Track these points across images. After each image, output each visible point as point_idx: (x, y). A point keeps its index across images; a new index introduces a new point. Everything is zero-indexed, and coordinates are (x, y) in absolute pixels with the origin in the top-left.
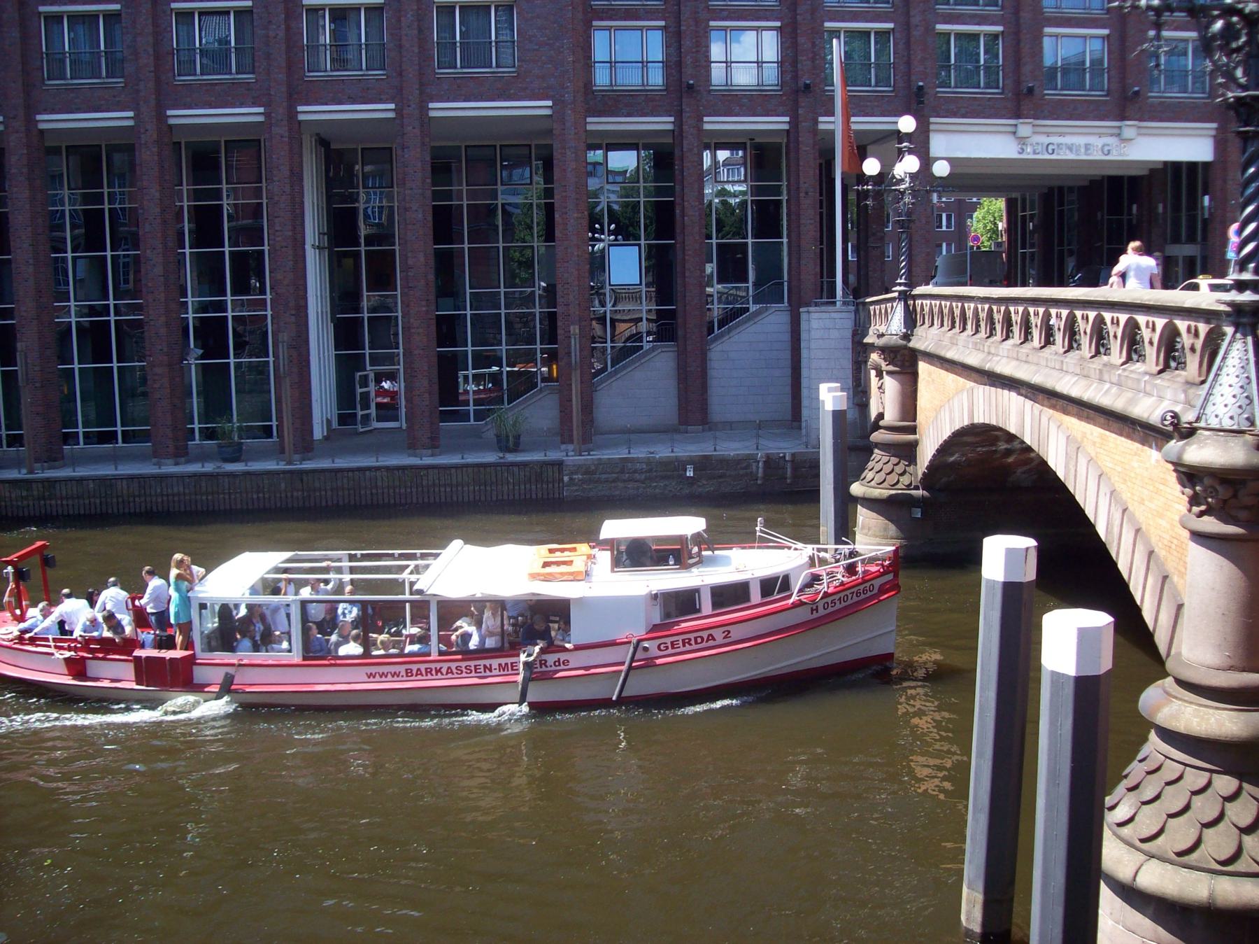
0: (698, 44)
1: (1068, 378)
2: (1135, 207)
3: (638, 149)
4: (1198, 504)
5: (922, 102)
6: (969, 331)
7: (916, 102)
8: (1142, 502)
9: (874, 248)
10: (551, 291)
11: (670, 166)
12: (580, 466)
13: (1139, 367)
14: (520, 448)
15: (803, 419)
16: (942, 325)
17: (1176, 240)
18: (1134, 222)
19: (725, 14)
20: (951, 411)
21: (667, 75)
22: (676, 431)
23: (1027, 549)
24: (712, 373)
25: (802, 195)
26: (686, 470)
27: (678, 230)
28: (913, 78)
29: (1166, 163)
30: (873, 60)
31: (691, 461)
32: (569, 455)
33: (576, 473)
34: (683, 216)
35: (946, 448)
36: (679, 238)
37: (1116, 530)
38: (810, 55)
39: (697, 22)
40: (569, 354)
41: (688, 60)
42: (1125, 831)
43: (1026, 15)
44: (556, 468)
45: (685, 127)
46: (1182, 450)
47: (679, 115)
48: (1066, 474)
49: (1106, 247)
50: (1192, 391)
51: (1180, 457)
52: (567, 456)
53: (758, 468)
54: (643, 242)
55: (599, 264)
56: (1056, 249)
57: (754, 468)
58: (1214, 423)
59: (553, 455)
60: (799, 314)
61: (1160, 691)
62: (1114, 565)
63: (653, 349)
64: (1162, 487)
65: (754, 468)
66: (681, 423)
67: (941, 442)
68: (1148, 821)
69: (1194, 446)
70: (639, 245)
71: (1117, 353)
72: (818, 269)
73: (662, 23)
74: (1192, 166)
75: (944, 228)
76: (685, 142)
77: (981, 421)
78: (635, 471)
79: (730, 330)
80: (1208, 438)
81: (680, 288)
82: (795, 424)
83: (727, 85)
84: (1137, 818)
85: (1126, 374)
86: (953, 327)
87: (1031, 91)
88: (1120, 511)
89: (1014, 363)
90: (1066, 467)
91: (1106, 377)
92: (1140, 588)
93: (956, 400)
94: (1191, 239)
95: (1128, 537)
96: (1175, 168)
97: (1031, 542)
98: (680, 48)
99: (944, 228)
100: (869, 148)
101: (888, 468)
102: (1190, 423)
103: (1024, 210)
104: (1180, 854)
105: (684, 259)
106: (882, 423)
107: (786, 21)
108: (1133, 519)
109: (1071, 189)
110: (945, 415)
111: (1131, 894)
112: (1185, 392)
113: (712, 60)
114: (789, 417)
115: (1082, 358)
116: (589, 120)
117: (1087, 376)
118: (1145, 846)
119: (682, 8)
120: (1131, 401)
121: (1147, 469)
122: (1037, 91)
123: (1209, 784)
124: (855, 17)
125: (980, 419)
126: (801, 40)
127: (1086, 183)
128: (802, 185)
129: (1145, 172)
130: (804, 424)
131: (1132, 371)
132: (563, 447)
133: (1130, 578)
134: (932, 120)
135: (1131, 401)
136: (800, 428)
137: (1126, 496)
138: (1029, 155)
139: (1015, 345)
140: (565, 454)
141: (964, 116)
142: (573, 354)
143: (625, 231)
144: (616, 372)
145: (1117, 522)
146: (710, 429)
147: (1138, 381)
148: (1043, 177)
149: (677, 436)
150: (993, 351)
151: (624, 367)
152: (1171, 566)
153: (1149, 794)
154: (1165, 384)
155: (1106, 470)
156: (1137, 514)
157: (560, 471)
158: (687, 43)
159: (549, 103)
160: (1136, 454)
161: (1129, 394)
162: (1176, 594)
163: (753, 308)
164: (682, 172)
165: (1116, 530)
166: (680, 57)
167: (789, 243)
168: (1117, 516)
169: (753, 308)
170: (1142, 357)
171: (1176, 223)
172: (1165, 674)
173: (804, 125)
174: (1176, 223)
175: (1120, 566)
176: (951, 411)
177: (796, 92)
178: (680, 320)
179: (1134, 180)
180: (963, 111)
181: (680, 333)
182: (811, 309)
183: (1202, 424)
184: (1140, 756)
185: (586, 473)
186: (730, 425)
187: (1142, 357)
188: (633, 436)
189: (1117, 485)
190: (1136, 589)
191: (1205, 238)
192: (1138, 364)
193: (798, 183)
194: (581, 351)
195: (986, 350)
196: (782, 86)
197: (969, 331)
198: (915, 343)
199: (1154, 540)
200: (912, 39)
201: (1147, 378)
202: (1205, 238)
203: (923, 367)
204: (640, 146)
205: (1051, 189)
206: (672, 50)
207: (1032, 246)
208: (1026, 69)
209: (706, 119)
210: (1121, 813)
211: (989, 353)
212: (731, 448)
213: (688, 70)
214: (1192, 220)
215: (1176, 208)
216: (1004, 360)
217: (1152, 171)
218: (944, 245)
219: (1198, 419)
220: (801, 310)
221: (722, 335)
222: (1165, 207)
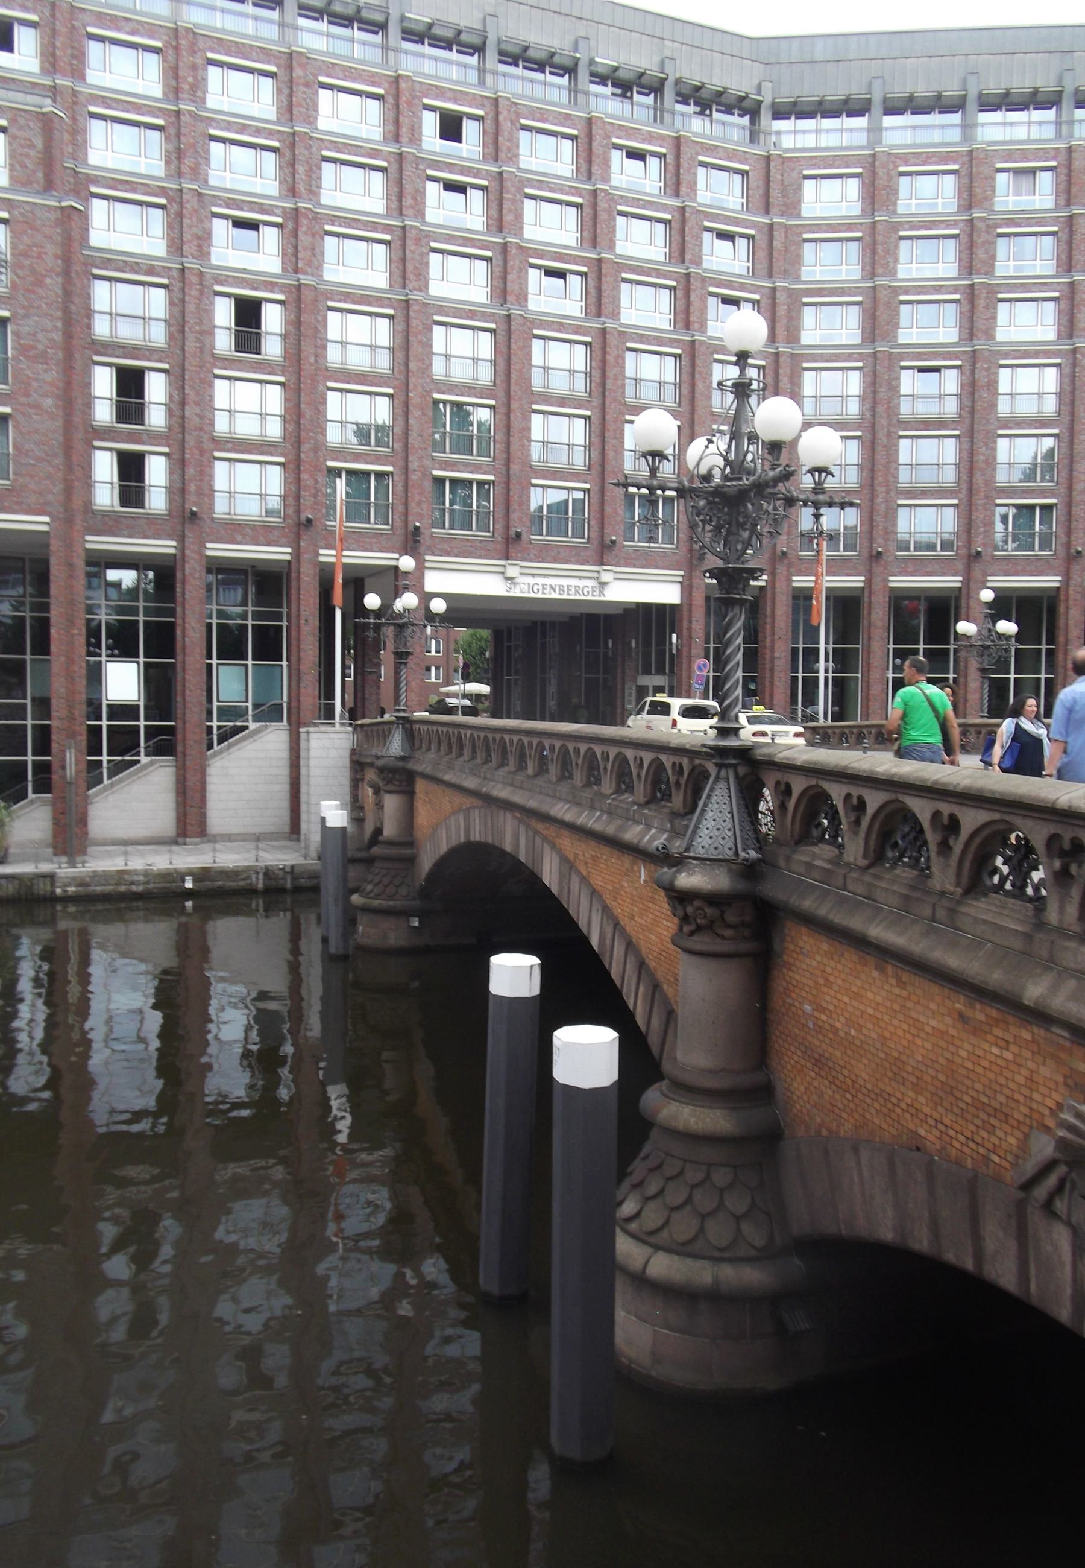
0: (202, 473)
1: (560, 805)
2: (610, 642)
3: (137, 569)
4: (689, 923)
5: (418, 541)
6: (466, 757)
7: (412, 542)
8: (632, 918)
9: (370, 673)
10: (43, 705)
11: (171, 588)
12: (74, 879)
13: (628, 798)
14: (10, 859)
15: (302, 832)
16: (439, 750)
17: (647, 671)
18: (610, 654)
19: (230, 446)
20: (448, 830)
21: (170, 500)
22: (176, 843)
23: (532, 966)
24: (210, 788)
25: (302, 622)
26: (184, 881)
27: (179, 650)
28: (410, 518)
29: (638, 604)
30: (372, 499)
31: (190, 872)
32: (63, 870)
33: (70, 885)
34: (184, 637)
35: (442, 864)
36: (180, 658)
37: (608, 942)
38: (313, 491)
39: (202, 452)
40: (64, 768)
41: (192, 487)
42: (633, 1226)
43: (515, 468)
44: (48, 881)
45: (187, 552)
46: (674, 877)
47: (182, 539)
48: (561, 890)
49: (584, 675)
50: (677, 821)
51: (672, 884)
52: (60, 868)
53: (257, 879)
54: (142, 659)
55: (95, 676)
56: (506, 644)
57: (254, 879)
58: (701, 852)
59: (45, 867)
60: (299, 732)
61: (658, 1094)
62: (608, 974)
63: (152, 763)
64: (650, 905)
65: (254, 879)
66: (178, 835)
67: (437, 857)
68: (653, 1217)
69: (683, 875)
70: (138, 663)
71: (607, 786)
72: (317, 693)
73: (166, 450)
74: (661, 608)
75: (433, 653)
76: (187, 566)
77: (478, 839)
78: (132, 883)
79: (229, 747)
80: (696, 866)
81: (180, 705)
82: (294, 836)
83: (229, 514)
84: (643, 1214)
85: (615, 803)
86: (450, 752)
87: (518, 535)
88: (612, 925)
89: (509, 789)
90: (560, 884)
91: (597, 805)
92: (633, 995)
93: (453, 821)
94: (660, 671)
95: (619, 950)
96: (646, 609)
97: (534, 960)
98: (183, 476)
99: (433, 653)
100: (368, 582)
101: (386, 881)
102: (680, 854)
103: (509, 640)
104: (683, 1244)
105: (184, 679)
106: (380, 838)
107: (290, 457)
108: (624, 933)
109: (553, 624)
110: (443, 834)
111: (641, 1281)
112: (671, 822)
113: (97, 395)
114: (287, 829)
115: (574, 787)
116: (88, 538)
117: (578, 804)
118: (652, 1239)
119: (187, 436)
120: (621, 828)
121: (636, 888)
122: (524, 536)
123: (681, 1173)
124: (357, 457)
125: (476, 836)
126: (304, 476)
127: (566, 619)
128: (302, 612)
129: (621, 612)
130: (302, 837)
131: (621, 801)
132: (55, 859)
133: (622, 985)
134: (427, 558)
135: (621, 828)
136: (298, 840)
137: (617, 911)
138: (516, 593)
139: (510, 772)
140: (57, 866)
141: (457, 556)
142: (68, 768)
143: (124, 649)
144: (112, 785)
145: (609, 936)
146: (209, 841)
147: (628, 810)
148: (529, 613)
149: (175, 848)
150: (488, 776)
151: (121, 781)
152: (660, 975)
153: (652, 1189)
154: (652, 813)
155: (599, 888)
156: (628, 929)
157: (53, 884)
158: (191, 471)
159: (47, 519)
160: (626, 875)
161: (619, 822)
162: (666, 1001)
163: (253, 726)
164: (184, 594)
165: (608, 942)
166: (184, 483)
167: (289, 666)
168: (609, 930)
169: (253, 726)
170: (630, 789)
171: (647, 656)
172: (659, 1076)
173: (306, 557)
174: (647, 656)
175: (613, 975)
176: (448, 830)
177: (299, 524)
178: (179, 736)
179: (608, 618)
180: (456, 551)
181: (180, 748)
182: (311, 729)
183: (691, 854)
184: (642, 1155)
185: (80, 885)
186: (229, 838)
187: (630, 789)
188: (130, 848)
189: (608, 902)
190: (629, 996)
191: (672, 670)
192: (626, 795)
193: (299, 611)
194: (76, 764)
195: (482, 775)
196: (284, 518)
197: (466, 757)
198: (411, 766)
199: (644, 951)
200: (410, 483)
201: (635, 808)
202: (672, 670)
203: (420, 785)
204: (141, 567)
205: (535, 623)
206: (176, 477)
207: (517, 673)
208: (514, 516)
209: (208, 545)
210: (628, 1208)
211: (485, 778)
212: (229, 858)
213: (191, 498)
214: (661, 654)
215: (647, 644)
216: (500, 786)
217: (625, 610)
218: (433, 669)
219: (687, 850)
220: (301, 730)
221: (221, 752)
222: (637, 643)
